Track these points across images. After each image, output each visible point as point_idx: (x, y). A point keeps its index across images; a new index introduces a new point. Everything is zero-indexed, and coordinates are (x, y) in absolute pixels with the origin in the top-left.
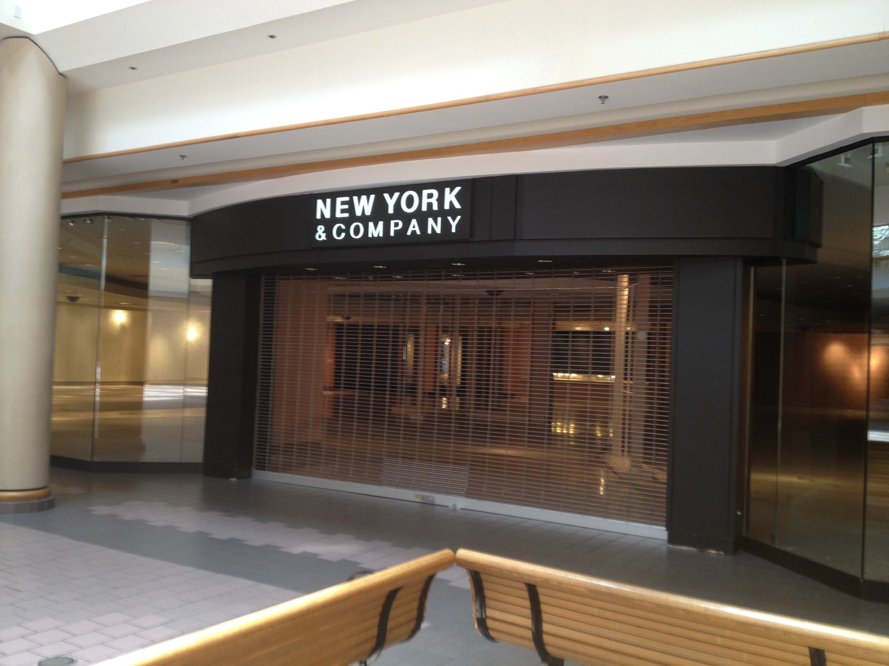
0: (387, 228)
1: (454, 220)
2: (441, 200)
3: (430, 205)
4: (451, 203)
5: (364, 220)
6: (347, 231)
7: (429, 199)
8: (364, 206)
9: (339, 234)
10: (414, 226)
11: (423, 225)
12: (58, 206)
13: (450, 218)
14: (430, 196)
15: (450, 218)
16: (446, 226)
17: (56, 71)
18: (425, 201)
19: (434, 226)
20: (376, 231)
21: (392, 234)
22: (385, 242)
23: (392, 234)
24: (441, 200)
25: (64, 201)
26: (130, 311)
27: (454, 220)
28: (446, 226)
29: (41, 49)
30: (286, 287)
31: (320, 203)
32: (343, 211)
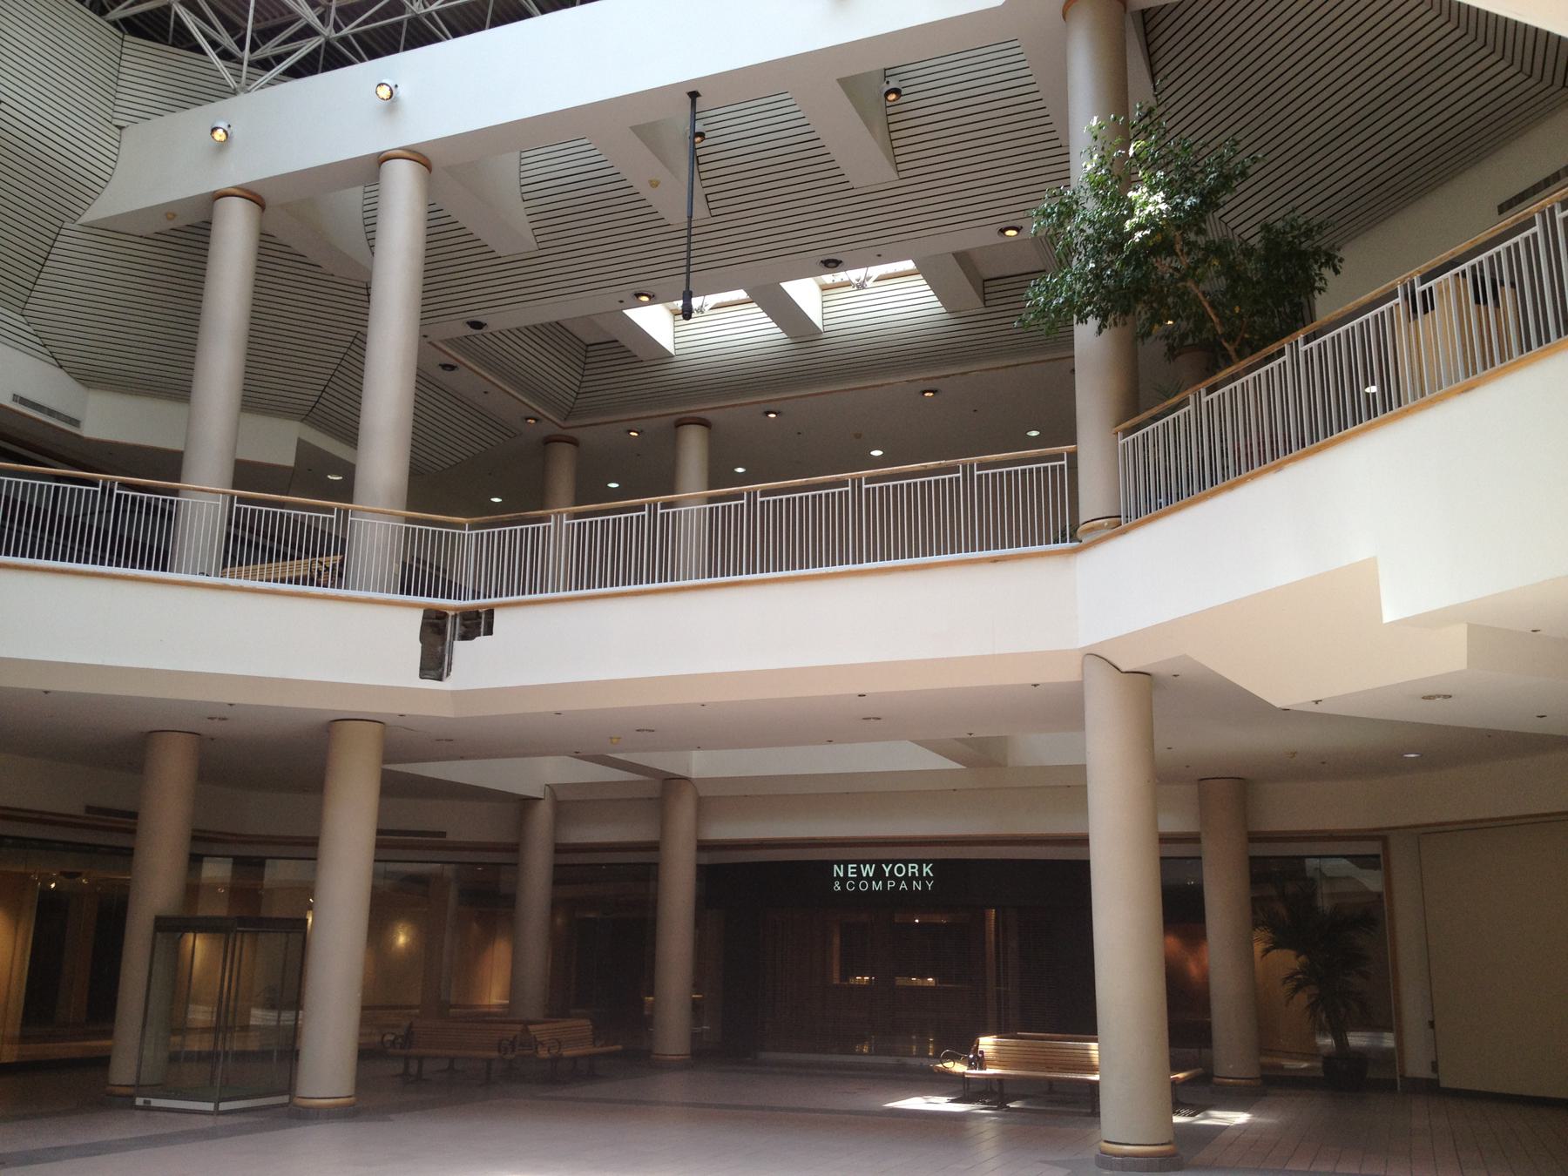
0: (885, 885)
1: (887, 867)
2: (921, 870)
3: (913, 873)
4: (927, 872)
5: (868, 878)
6: (857, 886)
7: (913, 869)
8: (868, 871)
10: (903, 885)
11: (909, 884)
13: (884, 866)
15: (884, 866)
16: (924, 886)
18: (910, 870)
19: (918, 886)
20: (877, 886)
24: (921, 870)
26: (205, 934)
27: (887, 867)
28: (924, 886)
30: (205, 859)
31: (836, 867)
32: (852, 873)
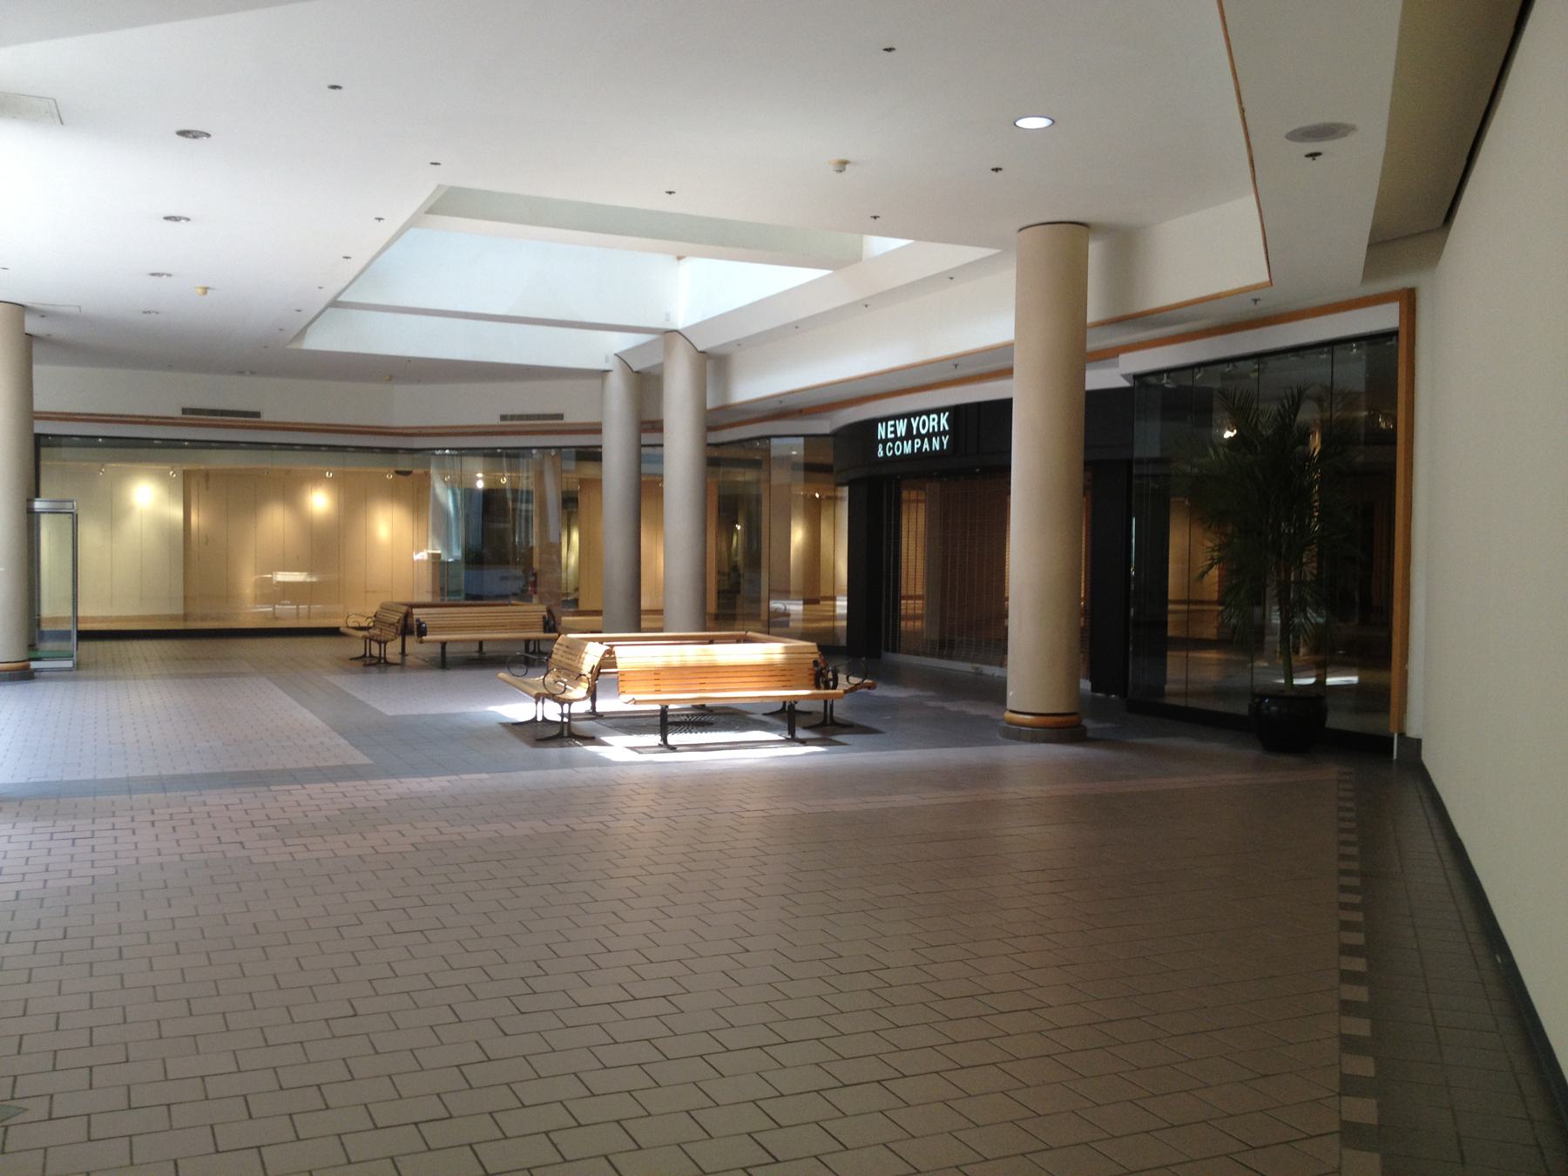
7: (932, 423)
8: (902, 428)
9: (889, 452)
12: (705, 438)
14: (934, 420)
17: (694, 351)
19: (936, 444)
21: (915, 451)
22: (912, 456)
23: (915, 451)
25: (709, 434)
29: (687, 339)
